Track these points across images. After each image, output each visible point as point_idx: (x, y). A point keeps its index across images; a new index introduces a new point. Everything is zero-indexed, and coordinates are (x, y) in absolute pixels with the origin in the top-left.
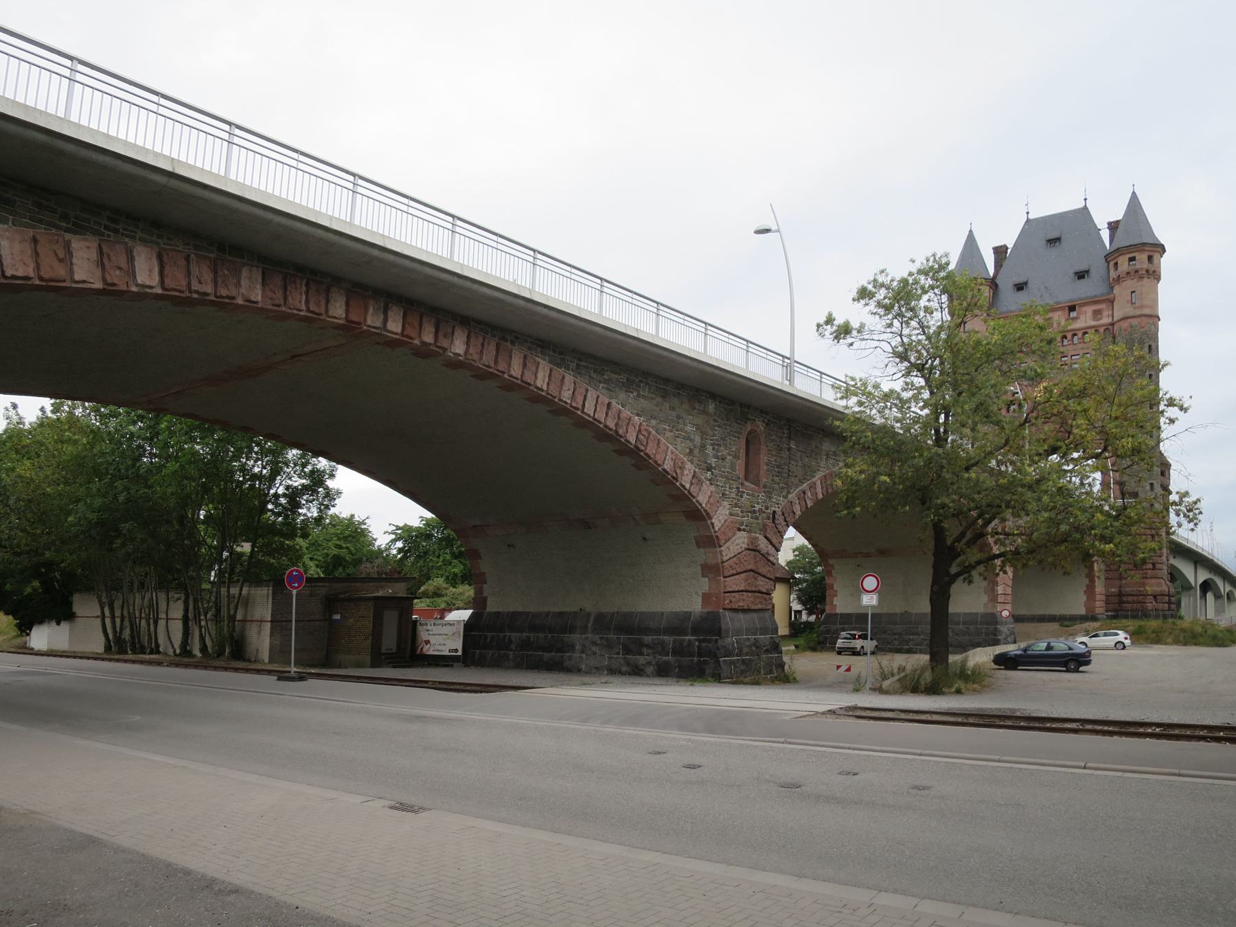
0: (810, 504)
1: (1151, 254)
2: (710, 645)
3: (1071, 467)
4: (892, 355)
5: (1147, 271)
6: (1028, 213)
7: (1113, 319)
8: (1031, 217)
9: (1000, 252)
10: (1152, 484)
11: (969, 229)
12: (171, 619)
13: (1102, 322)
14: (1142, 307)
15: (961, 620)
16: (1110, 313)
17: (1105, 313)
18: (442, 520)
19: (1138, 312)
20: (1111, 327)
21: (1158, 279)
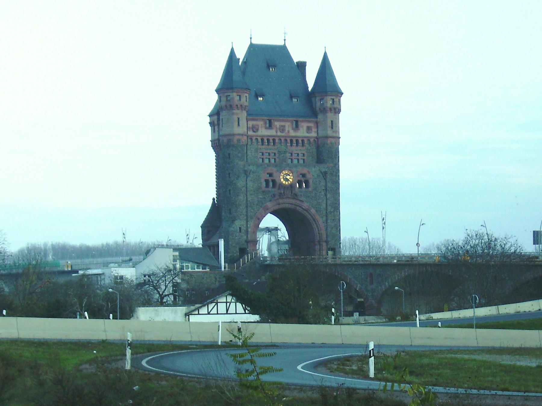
8: (254, 42)
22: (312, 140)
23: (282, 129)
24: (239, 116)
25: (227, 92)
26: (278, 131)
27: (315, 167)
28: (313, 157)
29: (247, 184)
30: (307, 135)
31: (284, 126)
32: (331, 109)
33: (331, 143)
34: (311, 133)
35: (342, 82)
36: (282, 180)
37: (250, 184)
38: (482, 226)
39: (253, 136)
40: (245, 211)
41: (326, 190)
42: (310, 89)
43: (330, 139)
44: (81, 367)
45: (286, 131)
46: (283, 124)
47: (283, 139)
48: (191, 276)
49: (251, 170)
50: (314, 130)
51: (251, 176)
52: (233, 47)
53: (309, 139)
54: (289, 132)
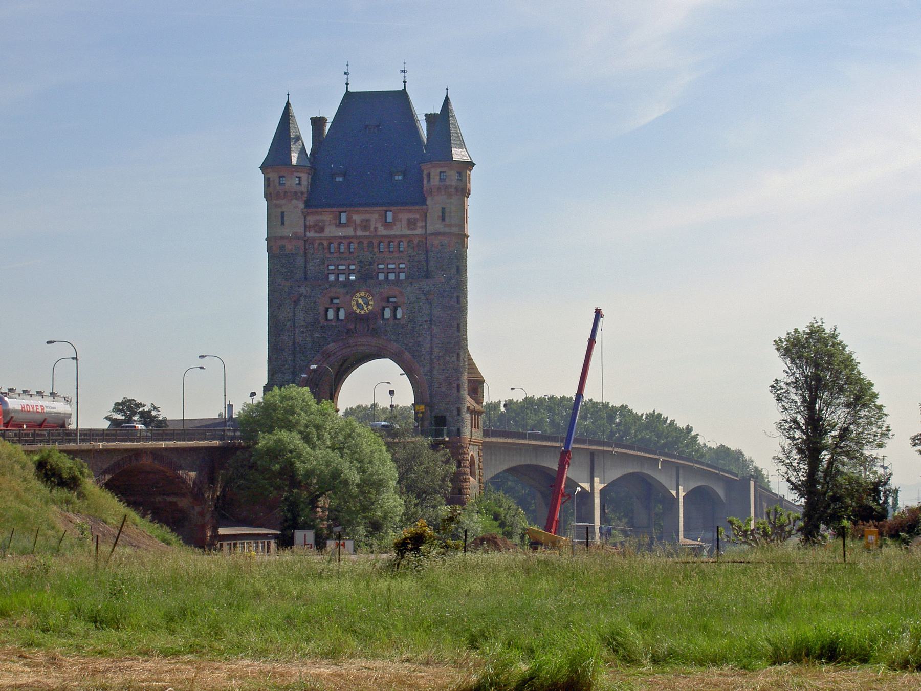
2: (526, 525)
3: (623, 677)
4: (324, 359)
5: (456, 188)
6: (347, 84)
7: (426, 231)
8: (351, 89)
13: (416, 232)
16: (424, 224)
17: (419, 224)
19: (447, 230)
23: (365, 225)
24: (284, 209)
26: (359, 229)
27: (412, 285)
28: (420, 268)
30: (409, 232)
31: (368, 221)
32: (439, 189)
34: (414, 229)
36: (355, 308)
37: (300, 315)
40: (290, 358)
41: (431, 321)
45: (372, 229)
46: (367, 216)
48: (914, 586)
49: (303, 293)
51: (302, 303)
52: (290, 101)
53: (410, 239)
54: (376, 229)
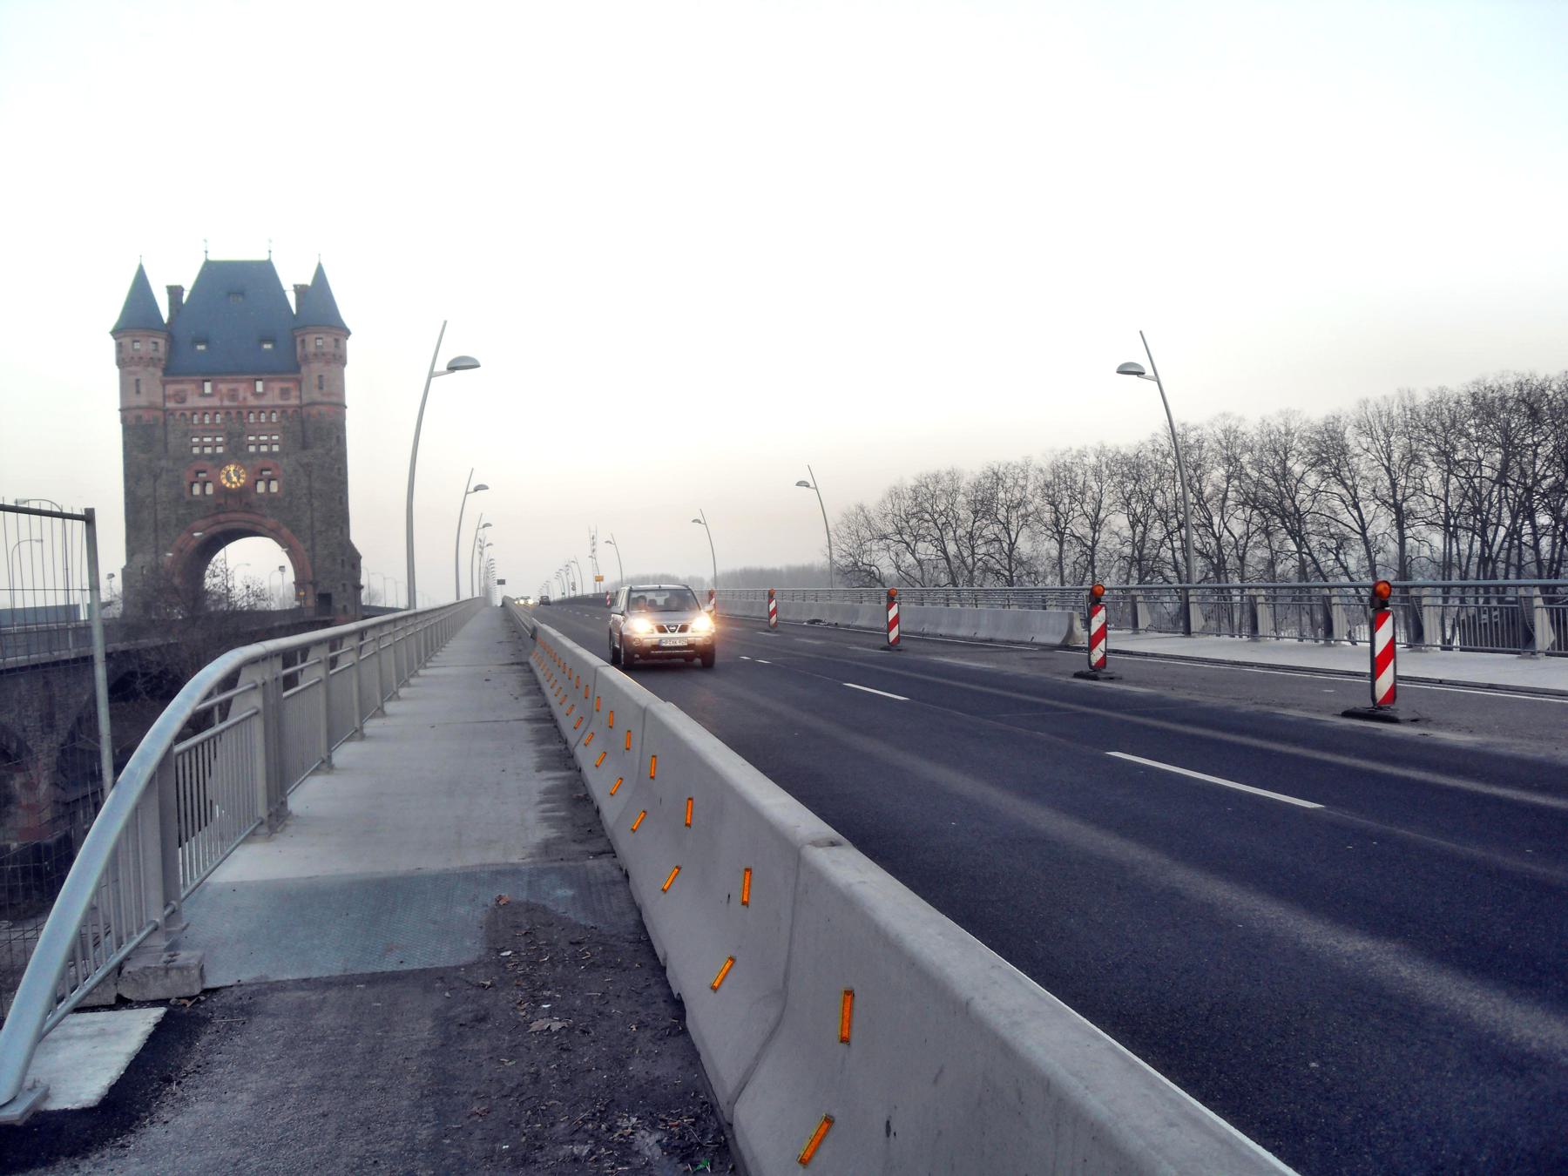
0: (230, 609)
1: (337, 337)
9: (175, 292)
10: (344, 585)
11: (139, 262)
12: (36, 620)
14: (329, 394)
15: (8, 911)
17: (294, 393)
18: (234, 611)
19: (326, 399)
20: (299, 410)
21: (344, 364)
22: (290, 411)
25: (154, 337)
29: (155, 490)
33: (320, 414)
35: (348, 312)
37: (162, 491)
38: (607, 542)
39: (176, 410)
42: (165, 320)
43: (317, 407)
44: (451, 1014)
47: (234, 413)
50: (294, 393)
54: (245, 399)
